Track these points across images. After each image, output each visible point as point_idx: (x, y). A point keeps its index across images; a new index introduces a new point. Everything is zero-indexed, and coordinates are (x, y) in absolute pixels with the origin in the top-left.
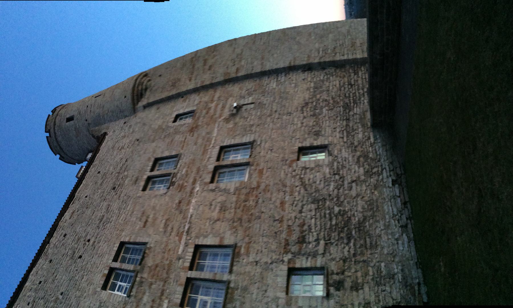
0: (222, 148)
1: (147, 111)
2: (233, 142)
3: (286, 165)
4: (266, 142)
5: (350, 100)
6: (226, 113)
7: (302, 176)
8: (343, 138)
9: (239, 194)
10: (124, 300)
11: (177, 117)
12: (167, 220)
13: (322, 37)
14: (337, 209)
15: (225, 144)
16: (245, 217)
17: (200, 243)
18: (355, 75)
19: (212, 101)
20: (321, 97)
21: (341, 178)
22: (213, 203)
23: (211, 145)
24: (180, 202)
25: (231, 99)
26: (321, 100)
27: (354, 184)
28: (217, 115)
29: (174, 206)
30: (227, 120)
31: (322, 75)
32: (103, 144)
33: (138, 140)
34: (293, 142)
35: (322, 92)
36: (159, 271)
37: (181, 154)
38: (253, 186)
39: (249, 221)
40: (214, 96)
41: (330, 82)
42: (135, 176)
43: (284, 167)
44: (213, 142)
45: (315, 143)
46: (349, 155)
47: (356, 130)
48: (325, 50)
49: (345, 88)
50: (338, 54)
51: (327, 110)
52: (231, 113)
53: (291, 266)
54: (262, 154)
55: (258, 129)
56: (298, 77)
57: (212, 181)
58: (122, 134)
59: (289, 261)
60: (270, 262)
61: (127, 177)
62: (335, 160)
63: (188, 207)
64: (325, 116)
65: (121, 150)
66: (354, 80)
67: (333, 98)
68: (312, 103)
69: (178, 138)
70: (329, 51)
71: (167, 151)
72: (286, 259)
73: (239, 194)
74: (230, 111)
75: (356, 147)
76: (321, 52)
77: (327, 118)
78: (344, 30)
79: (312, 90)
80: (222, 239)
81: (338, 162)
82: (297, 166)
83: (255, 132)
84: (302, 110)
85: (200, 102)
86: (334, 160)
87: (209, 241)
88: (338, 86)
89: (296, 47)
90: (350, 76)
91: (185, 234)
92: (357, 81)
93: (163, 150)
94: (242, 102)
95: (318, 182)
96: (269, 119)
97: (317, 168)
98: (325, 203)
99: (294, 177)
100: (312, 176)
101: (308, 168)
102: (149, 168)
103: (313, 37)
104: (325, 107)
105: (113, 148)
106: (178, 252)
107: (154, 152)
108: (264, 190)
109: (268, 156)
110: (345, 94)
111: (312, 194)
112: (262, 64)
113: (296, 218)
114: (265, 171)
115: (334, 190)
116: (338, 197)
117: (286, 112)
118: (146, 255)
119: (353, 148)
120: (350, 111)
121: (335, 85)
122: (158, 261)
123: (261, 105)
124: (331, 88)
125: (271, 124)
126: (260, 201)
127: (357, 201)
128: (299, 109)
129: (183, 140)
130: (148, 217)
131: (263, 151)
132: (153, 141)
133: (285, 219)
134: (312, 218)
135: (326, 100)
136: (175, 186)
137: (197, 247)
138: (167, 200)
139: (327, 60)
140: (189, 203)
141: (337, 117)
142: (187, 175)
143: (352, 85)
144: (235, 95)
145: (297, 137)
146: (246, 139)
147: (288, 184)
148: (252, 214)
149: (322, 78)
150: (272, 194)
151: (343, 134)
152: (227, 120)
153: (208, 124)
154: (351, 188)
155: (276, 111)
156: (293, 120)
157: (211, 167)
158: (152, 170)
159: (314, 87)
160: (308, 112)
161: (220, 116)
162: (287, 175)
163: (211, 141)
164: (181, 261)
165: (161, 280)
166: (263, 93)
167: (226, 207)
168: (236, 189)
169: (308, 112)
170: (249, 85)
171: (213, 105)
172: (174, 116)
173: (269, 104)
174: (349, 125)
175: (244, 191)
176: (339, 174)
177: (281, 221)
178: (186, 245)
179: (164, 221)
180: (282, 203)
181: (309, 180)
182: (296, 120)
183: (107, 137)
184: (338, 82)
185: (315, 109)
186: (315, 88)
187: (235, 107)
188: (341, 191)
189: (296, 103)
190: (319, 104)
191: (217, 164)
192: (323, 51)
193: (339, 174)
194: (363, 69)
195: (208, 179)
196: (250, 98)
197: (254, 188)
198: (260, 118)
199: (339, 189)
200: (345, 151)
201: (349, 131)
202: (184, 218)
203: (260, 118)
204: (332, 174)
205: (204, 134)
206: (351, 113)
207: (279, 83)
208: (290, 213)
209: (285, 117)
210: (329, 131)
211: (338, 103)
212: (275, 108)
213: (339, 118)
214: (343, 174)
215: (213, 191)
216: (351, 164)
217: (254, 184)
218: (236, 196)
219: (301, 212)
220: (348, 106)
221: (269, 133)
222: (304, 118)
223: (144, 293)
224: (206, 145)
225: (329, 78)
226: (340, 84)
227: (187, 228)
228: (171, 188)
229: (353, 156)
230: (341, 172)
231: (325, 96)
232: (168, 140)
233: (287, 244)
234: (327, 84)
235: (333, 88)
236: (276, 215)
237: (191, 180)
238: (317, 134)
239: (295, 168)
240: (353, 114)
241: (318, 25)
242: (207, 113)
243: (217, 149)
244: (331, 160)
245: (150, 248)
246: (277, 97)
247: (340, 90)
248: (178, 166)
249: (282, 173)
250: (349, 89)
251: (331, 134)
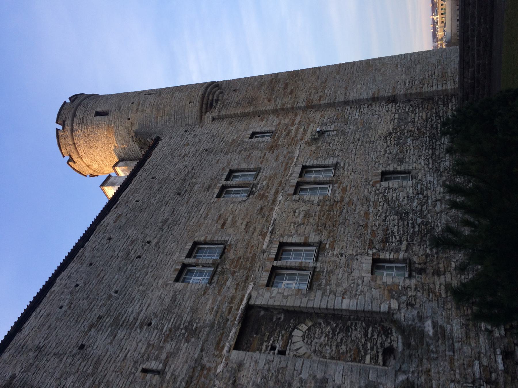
0: (304, 167)
1: (217, 124)
2: (315, 163)
3: (369, 184)
4: (349, 165)
5: (437, 131)
6: (308, 137)
7: (386, 194)
8: (428, 165)
9: (323, 206)
10: (204, 287)
11: (253, 135)
12: (248, 223)
13: (408, 68)
14: (419, 221)
15: (307, 164)
16: (329, 223)
17: (285, 241)
18: (444, 106)
19: (293, 125)
20: (405, 128)
21: (424, 197)
22: (297, 211)
23: (294, 163)
24: (262, 208)
25: (312, 125)
26: (406, 131)
27: (438, 203)
28: (299, 136)
29: (256, 211)
30: (309, 143)
31: (408, 107)
32: (156, 149)
33: (206, 151)
34: (376, 166)
35: (407, 123)
36: (242, 262)
37: (260, 168)
38: (336, 200)
39: (334, 226)
40: (294, 121)
41: (416, 114)
42: (206, 184)
43: (367, 187)
44: (295, 161)
45: (399, 169)
46: (434, 179)
47: (442, 158)
48: (412, 82)
49: (432, 120)
50: (426, 85)
51: (411, 140)
52: (313, 137)
53: (375, 257)
54: (345, 175)
55: (341, 153)
56: (382, 108)
57: (295, 193)
58: (184, 141)
59: (373, 254)
60: (355, 254)
61: (195, 184)
62: (418, 183)
63: (271, 213)
64: (409, 146)
65: (183, 157)
66: (443, 112)
67: (418, 129)
68: (397, 133)
69: (256, 154)
70: (416, 82)
71: (244, 164)
72: (370, 253)
73: (323, 206)
74: (312, 135)
75: (442, 172)
76: (407, 84)
77: (411, 147)
78: (433, 60)
79: (396, 121)
80: (306, 238)
81: (422, 185)
82: (380, 186)
83: (338, 156)
84: (386, 138)
85: (279, 123)
86: (417, 184)
87: (294, 239)
88: (424, 117)
89: (380, 78)
90: (439, 107)
91: (268, 233)
92: (447, 112)
93: (237, 161)
94: (324, 128)
95: (401, 200)
96: (351, 146)
97: (400, 189)
98: (408, 215)
99: (378, 195)
100: (395, 195)
101: (391, 188)
102: (224, 178)
103: (399, 69)
104: (410, 137)
105: (172, 154)
106: (262, 247)
107: (228, 164)
108: (348, 204)
109: (351, 177)
110: (432, 126)
111: (396, 208)
112: (345, 94)
113: (379, 225)
114: (348, 189)
115: (417, 207)
116: (421, 211)
117: (368, 140)
118: (226, 251)
119: (439, 173)
120: (437, 141)
121: (422, 117)
122: (240, 254)
123: (343, 133)
124: (416, 119)
125: (354, 150)
126: (344, 211)
127: (440, 216)
128: (383, 138)
129: (263, 155)
130: (226, 220)
131: (346, 172)
132: (227, 153)
133: (369, 225)
134: (394, 226)
135: (411, 131)
136: (255, 196)
137: (282, 245)
138: (246, 206)
139: (414, 91)
140: (272, 209)
141: (422, 146)
142: (268, 187)
143: (440, 117)
144: (317, 120)
145: (381, 162)
146: (330, 161)
147: (372, 199)
148: (336, 221)
149: (407, 110)
150: (356, 206)
151: (428, 161)
152: (309, 143)
153: (289, 145)
154: (435, 206)
155: (359, 140)
156: (376, 148)
157: (294, 182)
158: (227, 179)
159: (398, 118)
160: (391, 141)
161: (302, 140)
162: (370, 193)
163: (293, 160)
164: (265, 254)
165: (245, 268)
166: (346, 122)
167: (309, 214)
168: (320, 201)
169: (391, 141)
170: (331, 113)
171: (294, 128)
172: (250, 132)
173: (352, 132)
174: (435, 154)
175: (328, 203)
176: (423, 194)
177: (366, 226)
178: (271, 242)
179: (244, 223)
180: (367, 214)
181: (392, 197)
182: (379, 147)
183: (160, 142)
184: (424, 114)
185: (399, 139)
186: (400, 119)
187: (319, 132)
188: (425, 207)
189: (379, 132)
190: (404, 134)
191: (300, 179)
192: (409, 82)
193: (423, 194)
194: (454, 101)
195: (292, 191)
196: (333, 126)
197: (337, 202)
198: (343, 144)
199: (422, 206)
200: (430, 176)
201: (434, 158)
202: (267, 221)
203: (343, 144)
204: (415, 193)
205: (285, 152)
206: (438, 143)
207: (361, 114)
208: (374, 221)
209: (367, 145)
210: (413, 158)
211: (424, 134)
212: (357, 136)
213: (424, 148)
214: (427, 194)
215: (295, 201)
216: (435, 186)
217: (338, 198)
218: (320, 206)
219: (384, 221)
220: (434, 136)
221: (353, 158)
222: (388, 146)
223: (227, 279)
224: (288, 163)
225: (415, 110)
226: (426, 116)
227: (270, 229)
228: (251, 196)
229: (439, 180)
230: (425, 193)
231: (410, 126)
232: (245, 154)
233: (371, 242)
234: (413, 116)
235: (419, 120)
236: (360, 222)
237: (273, 191)
238: (401, 161)
239: (378, 187)
240: (439, 143)
241: (405, 55)
242: (288, 134)
243: (300, 167)
244: (414, 183)
245: (230, 245)
246: (360, 127)
247: (427, 121)
248: (258, 178)
249: (366, 190)
250: (436, 120)
251: (416, 160)
